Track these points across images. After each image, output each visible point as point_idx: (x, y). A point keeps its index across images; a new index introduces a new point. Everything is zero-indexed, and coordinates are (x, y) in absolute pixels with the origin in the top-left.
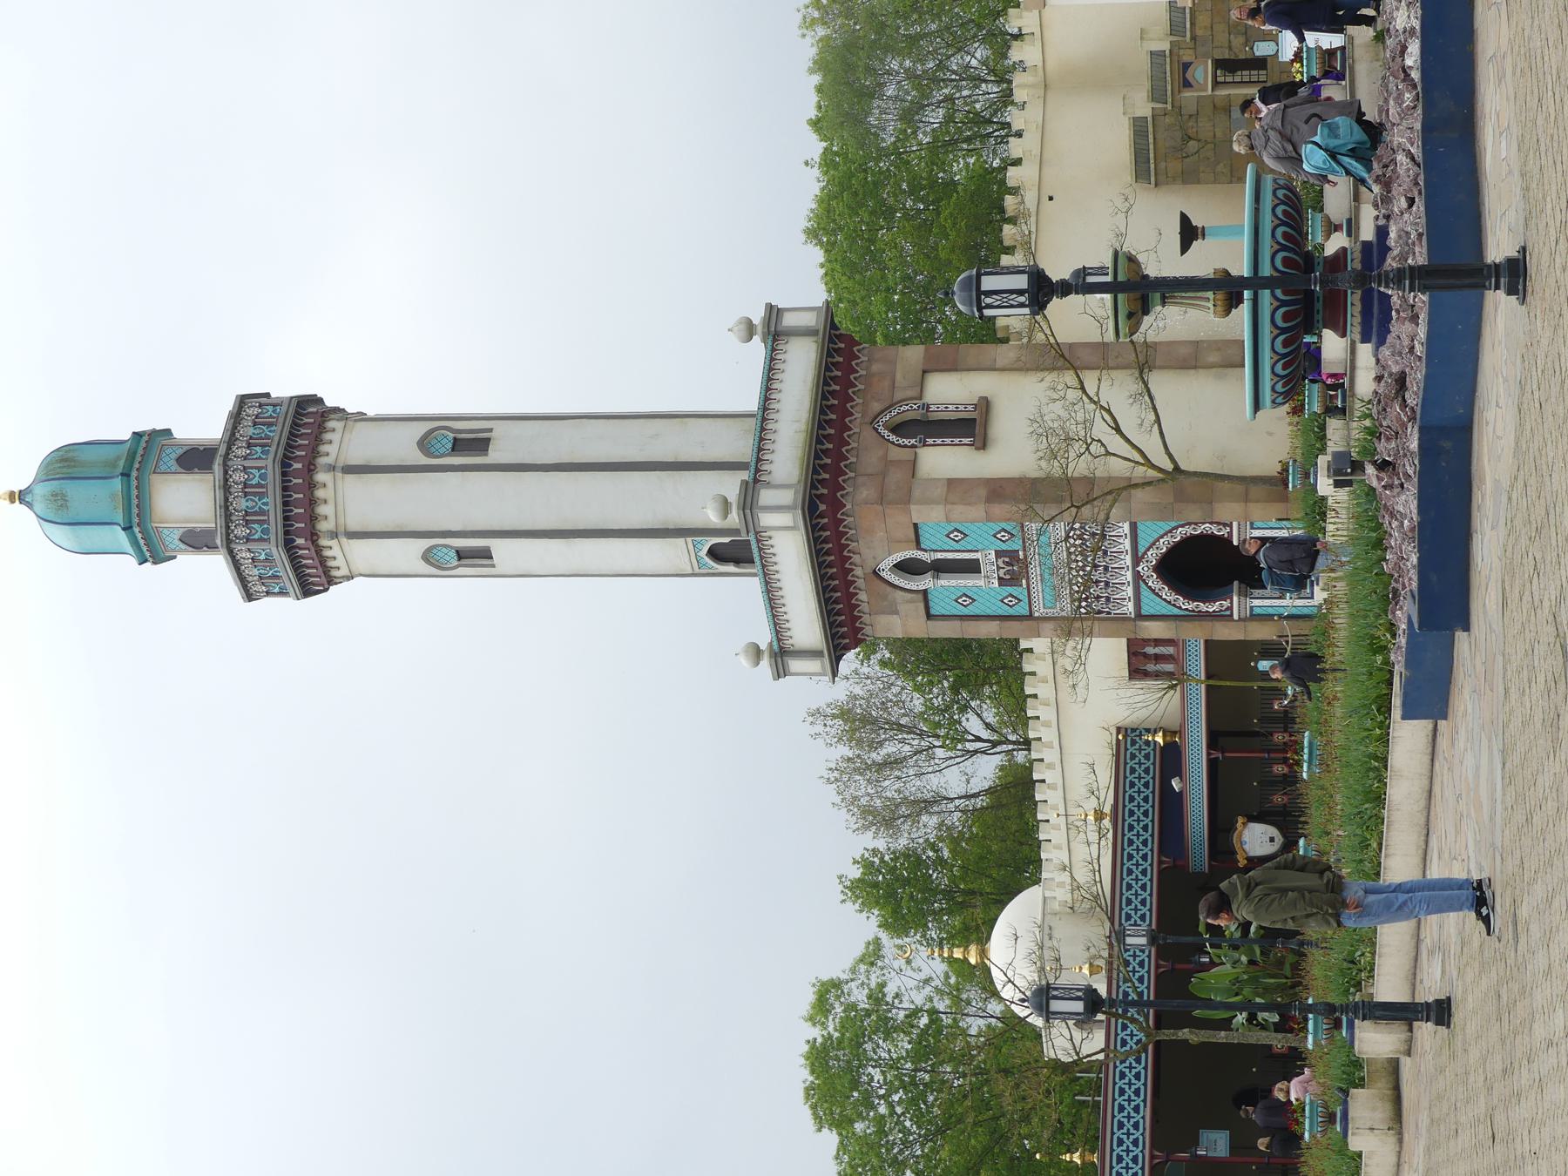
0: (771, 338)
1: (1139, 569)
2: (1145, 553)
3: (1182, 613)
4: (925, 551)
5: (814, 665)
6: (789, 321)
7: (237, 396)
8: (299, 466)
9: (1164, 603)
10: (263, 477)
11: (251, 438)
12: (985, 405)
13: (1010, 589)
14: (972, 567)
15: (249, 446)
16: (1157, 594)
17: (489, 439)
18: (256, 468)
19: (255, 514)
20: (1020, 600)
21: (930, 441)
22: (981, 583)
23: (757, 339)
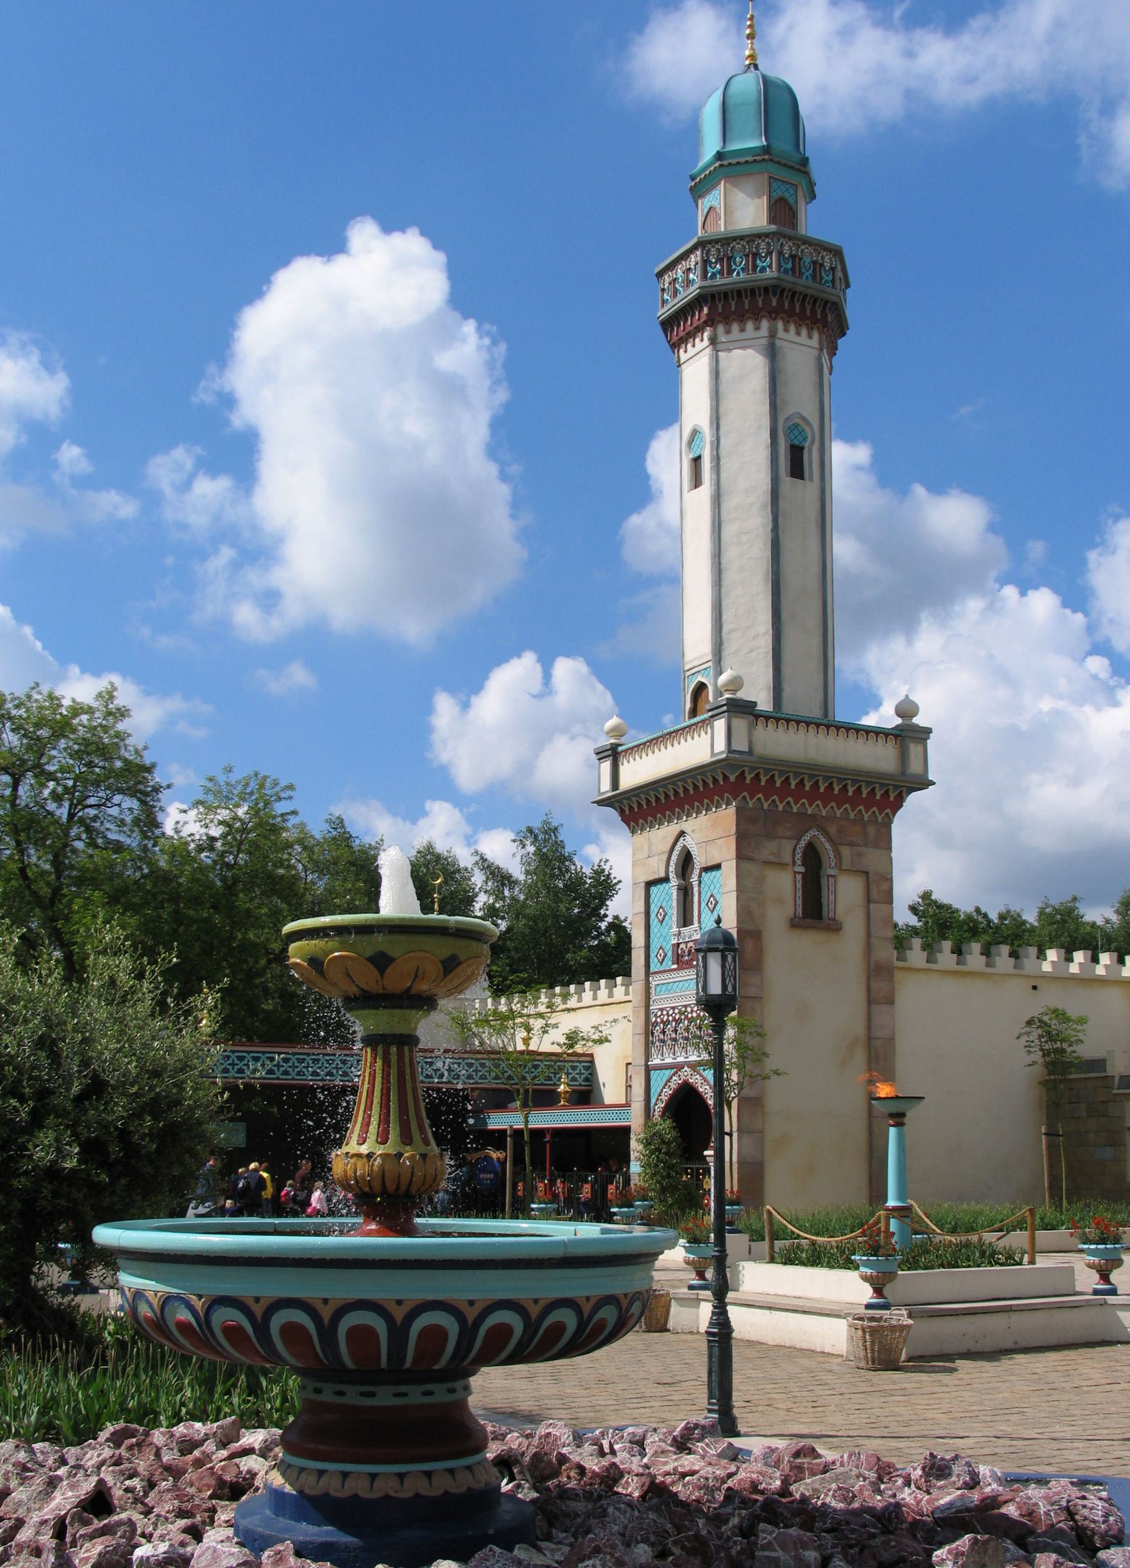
0: (898, 733)
1: (686, 1068)
2: (699, 1073)
3: (652, 1105)
4: (700, 876)
5: (606, 786)
6: (914, 749)
7: (841, 247)
8: (774, 303)
9: (659, 1091)
10: (763, 270)
11: (800, 259)
12: (835, 927)
13: (670, 954)
14: (686, 919)
15: (793, 257)
16: (666, 1084)
17: (803, 478)
18: (771, 263)
19: (729, 266)
20: (661, 964)
21: (799, 877)
22: (675, 929)
23: (899, 721)
